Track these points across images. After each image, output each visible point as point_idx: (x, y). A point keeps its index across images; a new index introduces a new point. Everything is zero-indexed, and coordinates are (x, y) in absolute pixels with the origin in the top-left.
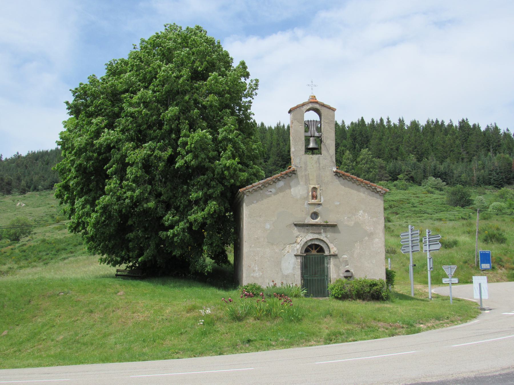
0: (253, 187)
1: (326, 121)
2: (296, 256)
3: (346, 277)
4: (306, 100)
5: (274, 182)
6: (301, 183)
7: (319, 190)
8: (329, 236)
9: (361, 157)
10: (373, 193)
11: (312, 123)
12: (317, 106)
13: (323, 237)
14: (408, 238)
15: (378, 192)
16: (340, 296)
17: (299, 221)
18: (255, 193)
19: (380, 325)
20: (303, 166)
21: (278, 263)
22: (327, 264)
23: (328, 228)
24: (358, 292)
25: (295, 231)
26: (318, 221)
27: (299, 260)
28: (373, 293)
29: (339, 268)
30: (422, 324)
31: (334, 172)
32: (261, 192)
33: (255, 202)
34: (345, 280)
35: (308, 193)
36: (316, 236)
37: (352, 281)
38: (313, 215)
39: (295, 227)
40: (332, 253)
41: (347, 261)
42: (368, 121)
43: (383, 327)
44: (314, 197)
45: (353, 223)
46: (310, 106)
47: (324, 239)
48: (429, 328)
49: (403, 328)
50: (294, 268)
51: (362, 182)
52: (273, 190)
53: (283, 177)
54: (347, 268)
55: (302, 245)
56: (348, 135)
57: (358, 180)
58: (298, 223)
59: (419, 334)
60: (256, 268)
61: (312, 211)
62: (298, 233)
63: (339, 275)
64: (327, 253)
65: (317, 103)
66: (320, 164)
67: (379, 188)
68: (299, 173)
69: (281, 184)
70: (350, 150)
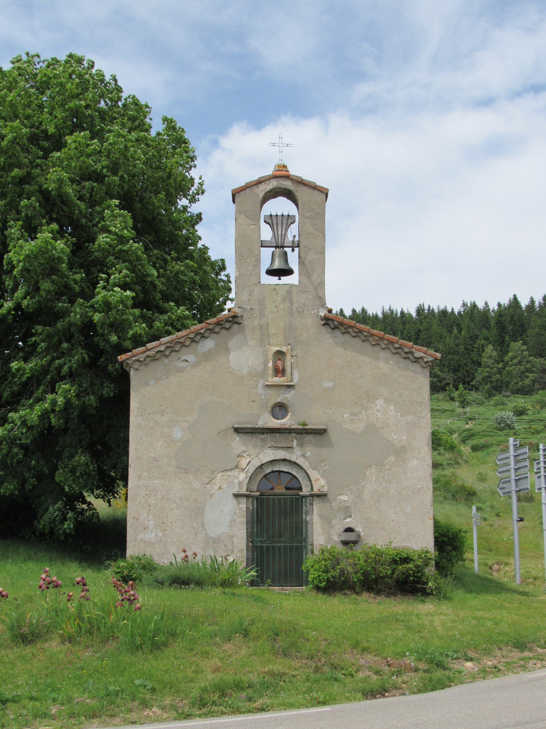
0: (148, 350)
1: (307, 215)
2: (237, 496)
3: (345, 543)
4: (269, 171)
5: (193, 341)
6: (251, 343)
7: (288, 356)
8: (308, 454)
9: (510, 354)
10: (407, 362)
11: (280, 219)
12: (288, 184)
13: (295, 456)
14: (508, 464)
15: (417, 360)
16: (323, 584)
17: (244, 423)
18: (154, 365)
19: (362, 662)
20: (256, 307)
21: (197, 512)
22: (307, 513)
23: (308, 438)
24: (366, 574)
25: (237, 443)
26: (286, 422)
27: (244, 506)
28: (401, 579)
29: (330, 523)
30: (471, 660)
31: (322, 320)
32: (166, 361)
33: (152, 382)
34: (340, 548)
35: (266, 363)
36: (281, 454)
37: (358, 550)
38: (277, 409)
39: (235, 435)
40: (316, 491)
41: (347, 507)
42: (524, 302)
43: (370, 668)
44: (279, 371)
45: (362, 425)
46: (273, 184)
47: (297, 461)
48: (484, 673)
49: (416, 670)
50: (232, 523)
51: (382, 339)
52: (191, 358)
53: (212, 331)
54: (349, 522)
55: (250, 474)
56: (493, 323)
57: (372, 335)
58: (242, 426)
59: (446, 692)
60: (151, 523)
61: (273, 402)
62: (243, 448)
63: (329, 539)
64: (305, 491)
65: (288, 177)
66: (291, 302)
67: (419, 351)
68: (246, 322)
69: (209, 344)
70: (493, 346)
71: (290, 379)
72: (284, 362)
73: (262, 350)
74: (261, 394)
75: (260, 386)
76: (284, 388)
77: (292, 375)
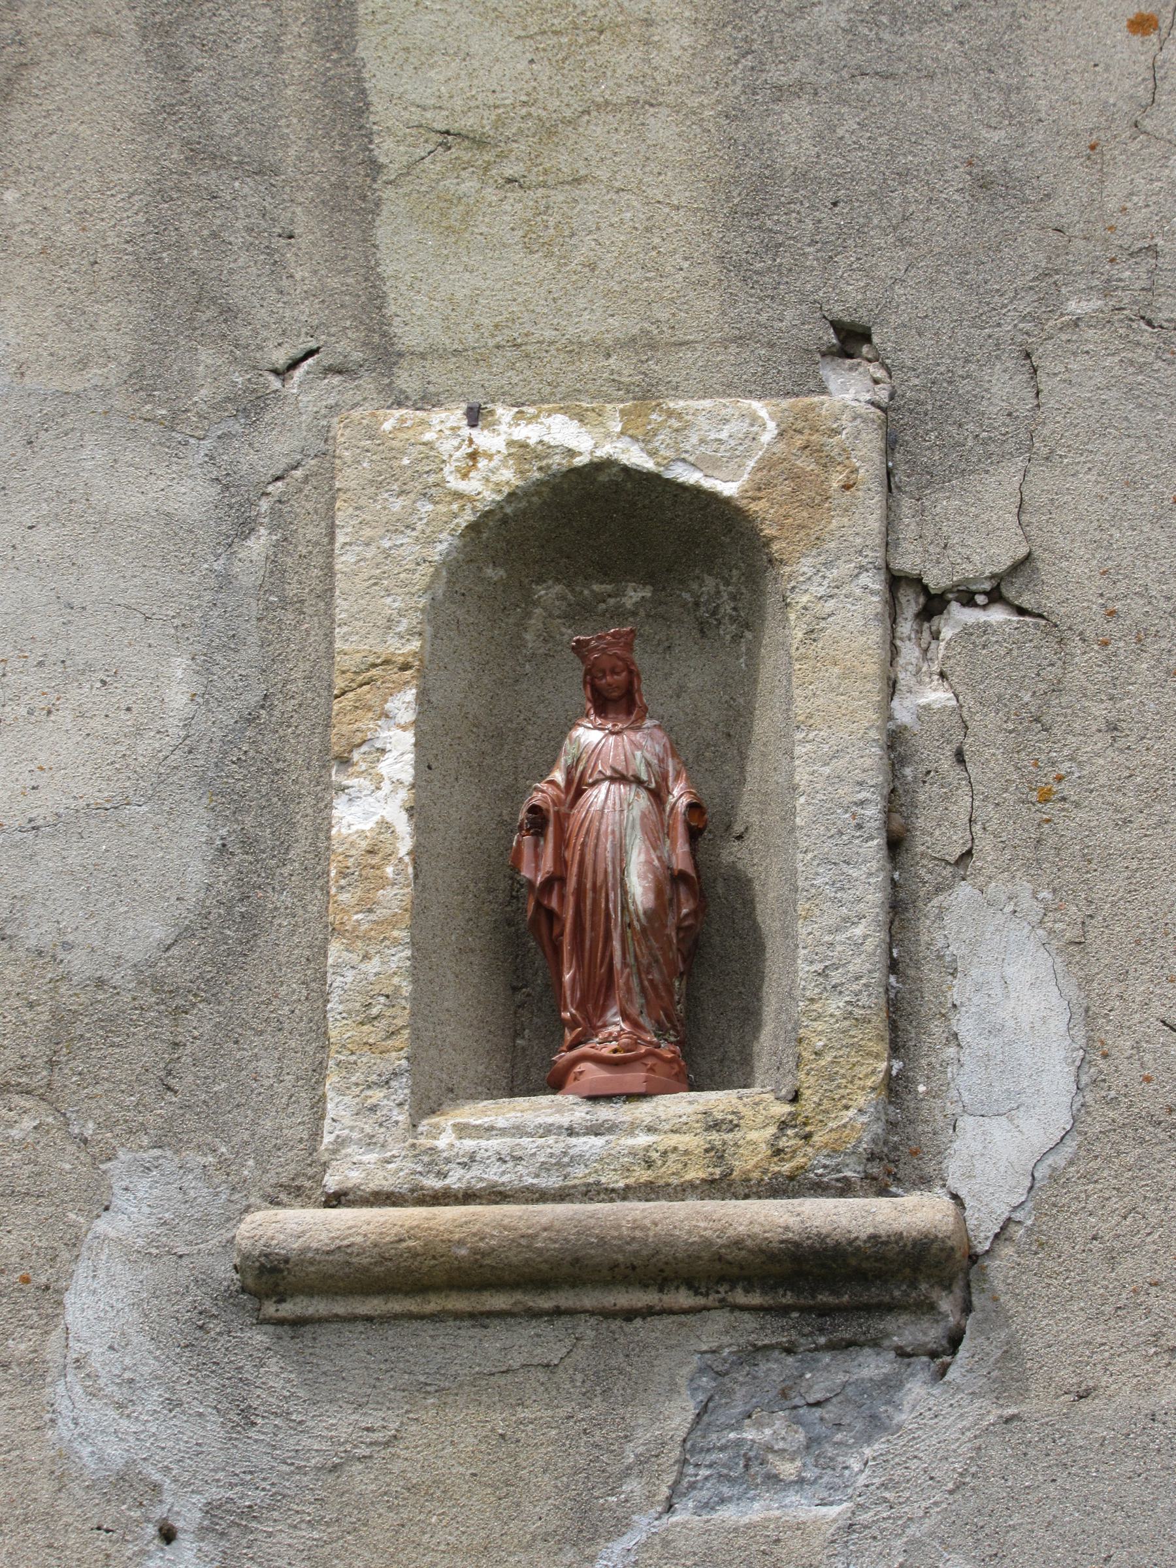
7: (825, 606)
35: (259, 784)
44: (598, 962)
71: (855, 1117)
72: (718, 745)
73: (191, 495)
74: (127, 1483)
75: (99, 1307)
76: (717, 1333)
77: (903, 1016)
